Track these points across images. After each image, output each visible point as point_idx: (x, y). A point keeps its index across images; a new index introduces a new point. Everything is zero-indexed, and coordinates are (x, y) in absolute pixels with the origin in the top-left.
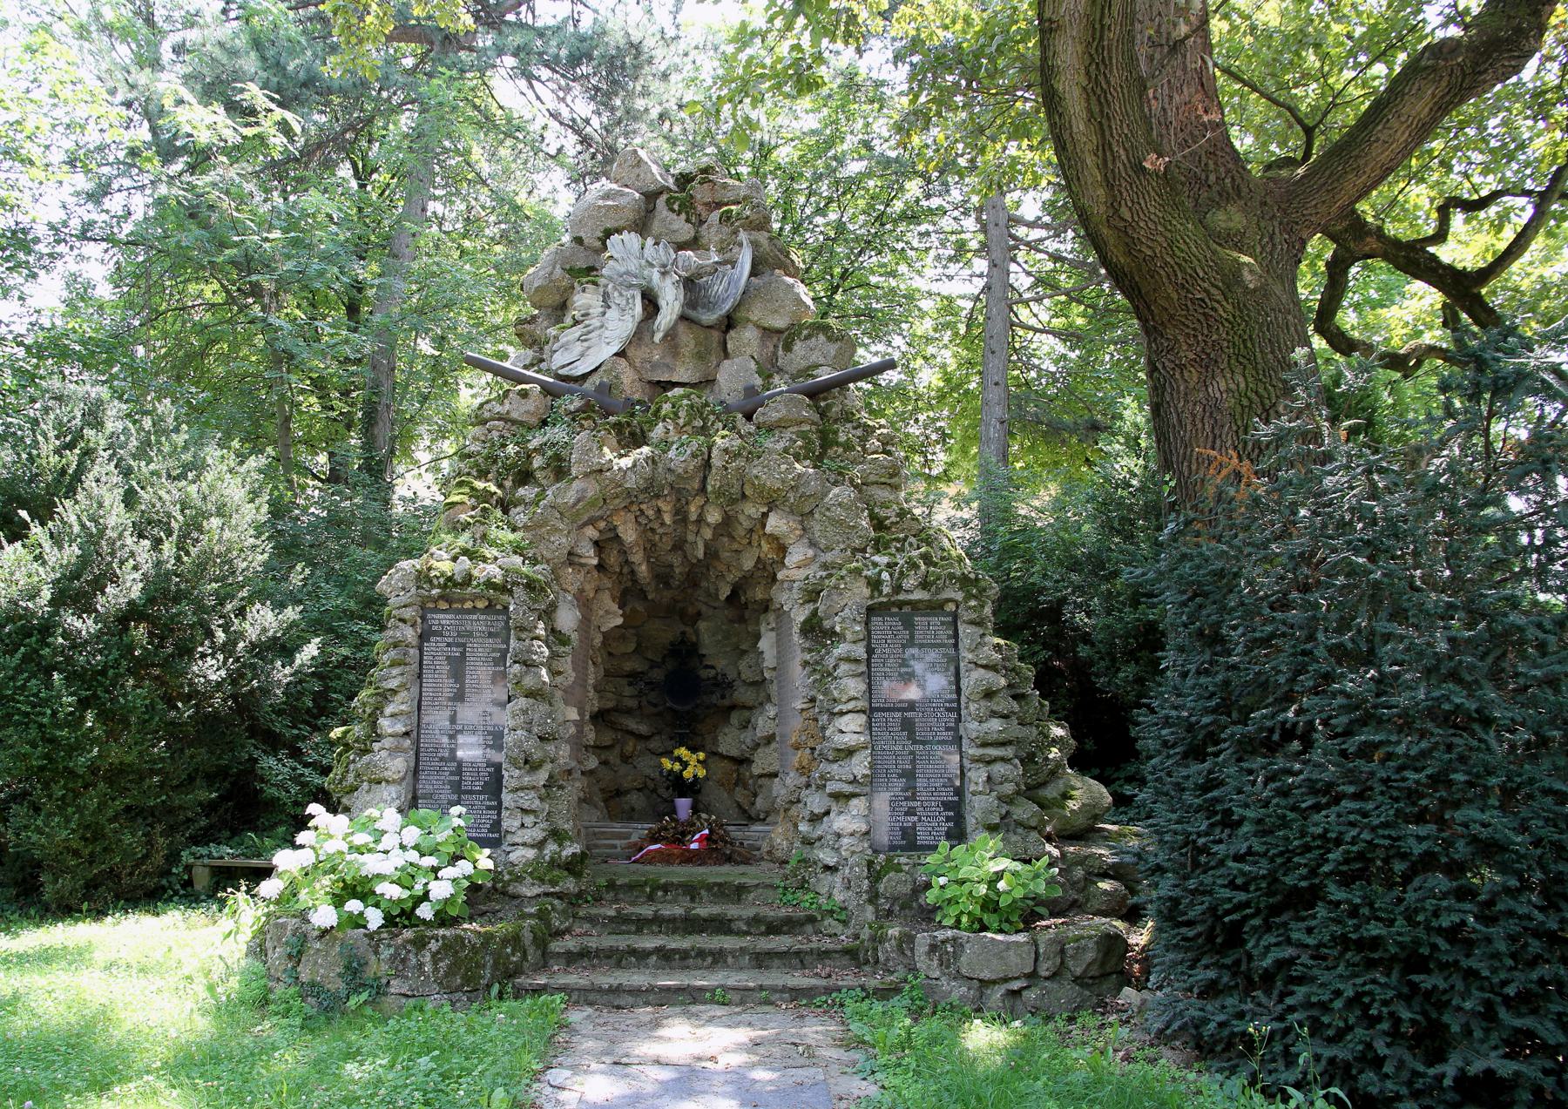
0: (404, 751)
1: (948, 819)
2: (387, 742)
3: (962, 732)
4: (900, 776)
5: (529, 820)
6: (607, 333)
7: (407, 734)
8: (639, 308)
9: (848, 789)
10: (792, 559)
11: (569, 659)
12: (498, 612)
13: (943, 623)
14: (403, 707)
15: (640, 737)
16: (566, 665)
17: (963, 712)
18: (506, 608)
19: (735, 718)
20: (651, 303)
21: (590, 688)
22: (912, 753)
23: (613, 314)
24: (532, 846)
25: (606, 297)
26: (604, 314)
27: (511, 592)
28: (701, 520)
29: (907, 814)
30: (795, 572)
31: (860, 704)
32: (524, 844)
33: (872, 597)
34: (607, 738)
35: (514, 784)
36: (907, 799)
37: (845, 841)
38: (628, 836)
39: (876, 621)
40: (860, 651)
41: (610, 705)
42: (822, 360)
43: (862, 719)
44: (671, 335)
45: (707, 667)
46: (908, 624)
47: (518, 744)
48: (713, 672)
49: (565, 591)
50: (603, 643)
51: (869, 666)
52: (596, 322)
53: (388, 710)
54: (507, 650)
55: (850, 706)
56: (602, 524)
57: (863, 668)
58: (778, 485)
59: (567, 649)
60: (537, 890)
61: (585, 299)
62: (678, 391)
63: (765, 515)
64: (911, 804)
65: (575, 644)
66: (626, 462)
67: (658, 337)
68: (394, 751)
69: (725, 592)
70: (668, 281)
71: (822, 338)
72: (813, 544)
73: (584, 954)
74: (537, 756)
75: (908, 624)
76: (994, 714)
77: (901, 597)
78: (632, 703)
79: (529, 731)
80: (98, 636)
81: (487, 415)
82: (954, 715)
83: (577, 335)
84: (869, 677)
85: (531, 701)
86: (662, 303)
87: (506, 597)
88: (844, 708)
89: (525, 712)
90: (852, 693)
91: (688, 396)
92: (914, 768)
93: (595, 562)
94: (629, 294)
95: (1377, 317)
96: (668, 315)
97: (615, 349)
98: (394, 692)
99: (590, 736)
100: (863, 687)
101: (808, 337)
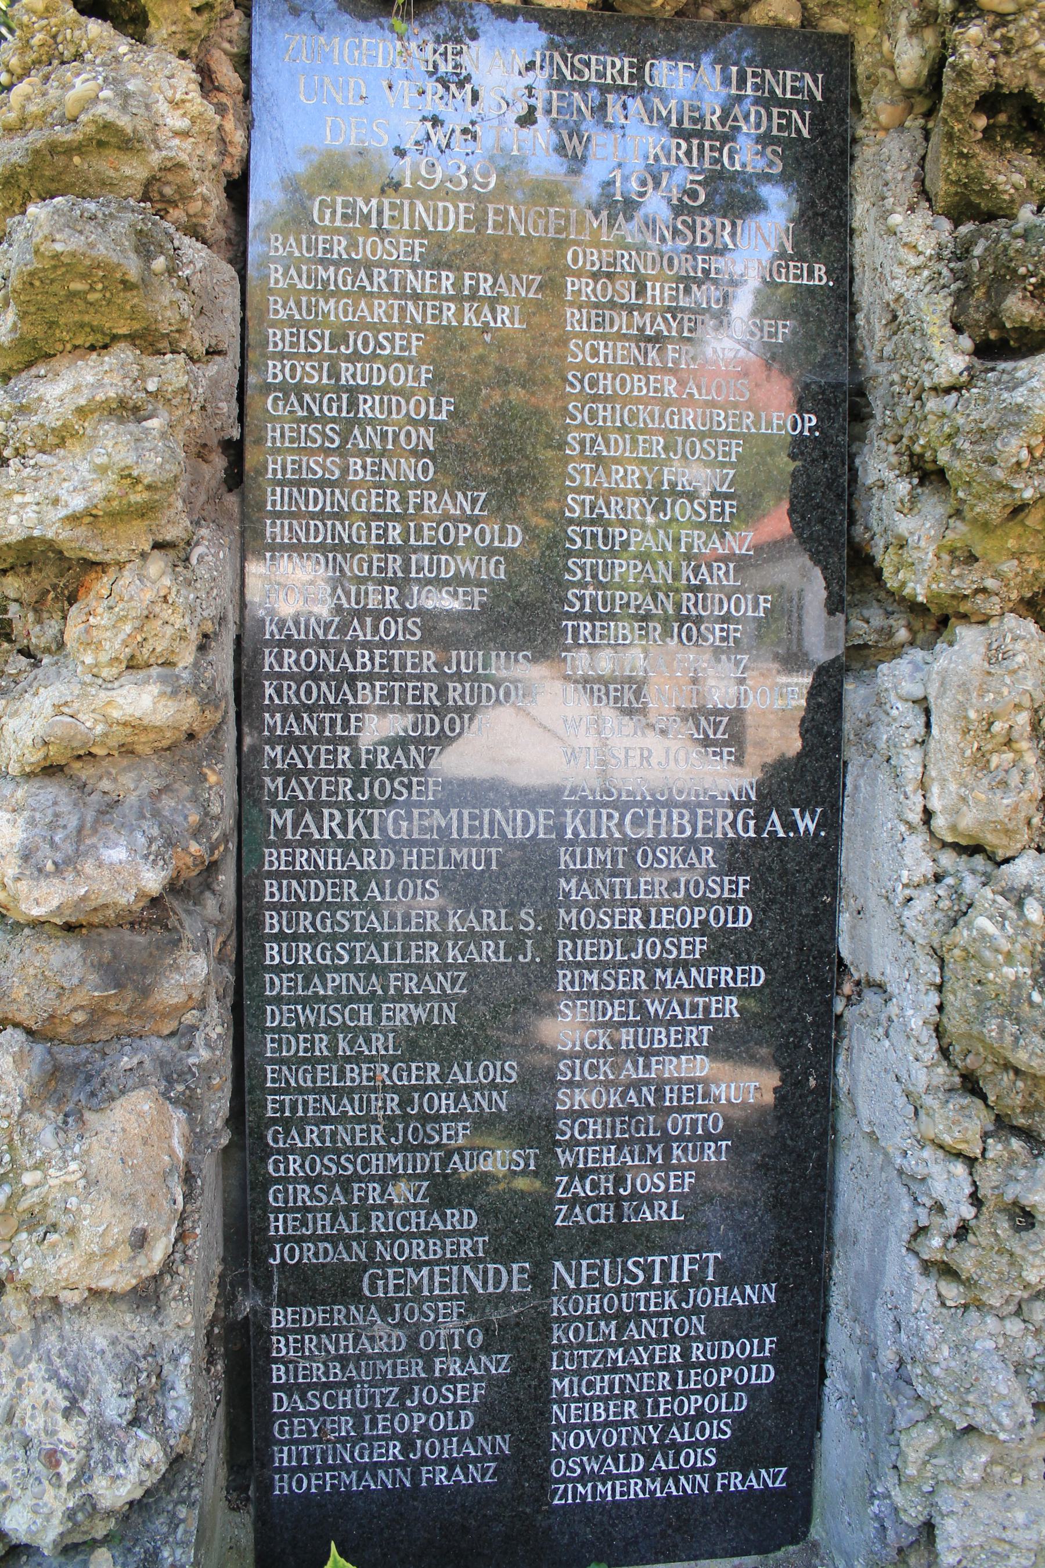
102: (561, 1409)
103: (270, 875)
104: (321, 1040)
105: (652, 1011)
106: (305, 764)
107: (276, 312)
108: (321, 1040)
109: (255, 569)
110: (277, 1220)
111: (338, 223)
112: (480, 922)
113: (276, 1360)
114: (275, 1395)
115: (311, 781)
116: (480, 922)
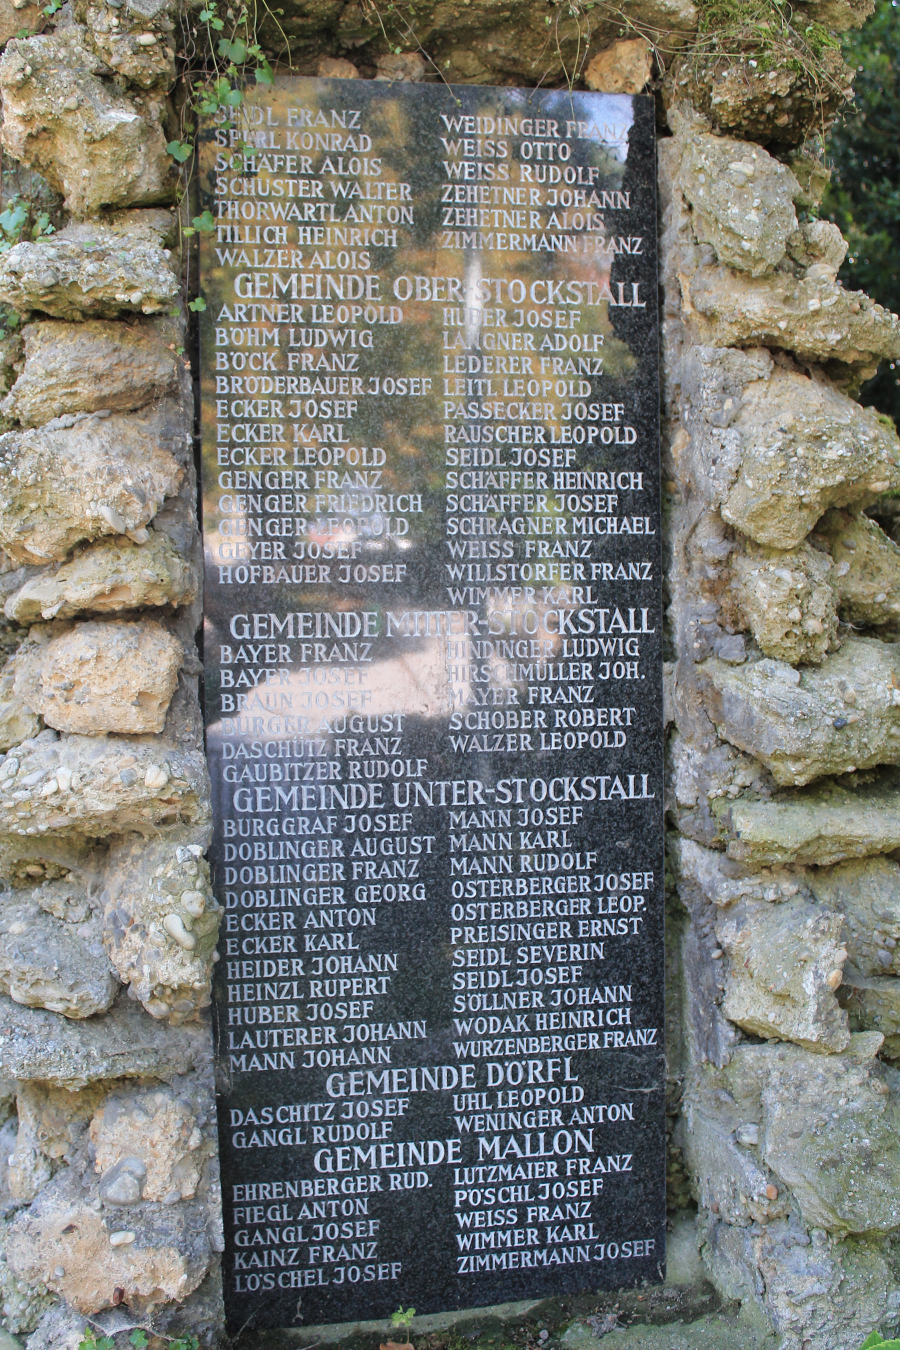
1: (607, 1138)
3: (676, 701)
4: (370, 941)
17: (688, 614)
22: (432, 821)
29: (404, 1130)
31: (138, 575)
43: (156, 657)
51: (196, 342)
55: (81, 584)
57: (157, 360)
66: (726, 98)
82: (635, 624)
88: (47, 594)
90: (95, 510)
92: (441, 899)
95: (169, 567)
100: (161, 476)
102: (491, 860)
103: (225, 691)
104: (297, 310)
105: (453, 552)
106: (251, 659)
107: (227, 682)
108: (297, 310)
109: (215, 728)
110: (233, 966)
111: (258, 295)
112: (331, 944)
113: (225, 691)
114: (227, 869)
115: (256, 672)
116: (331, 944)
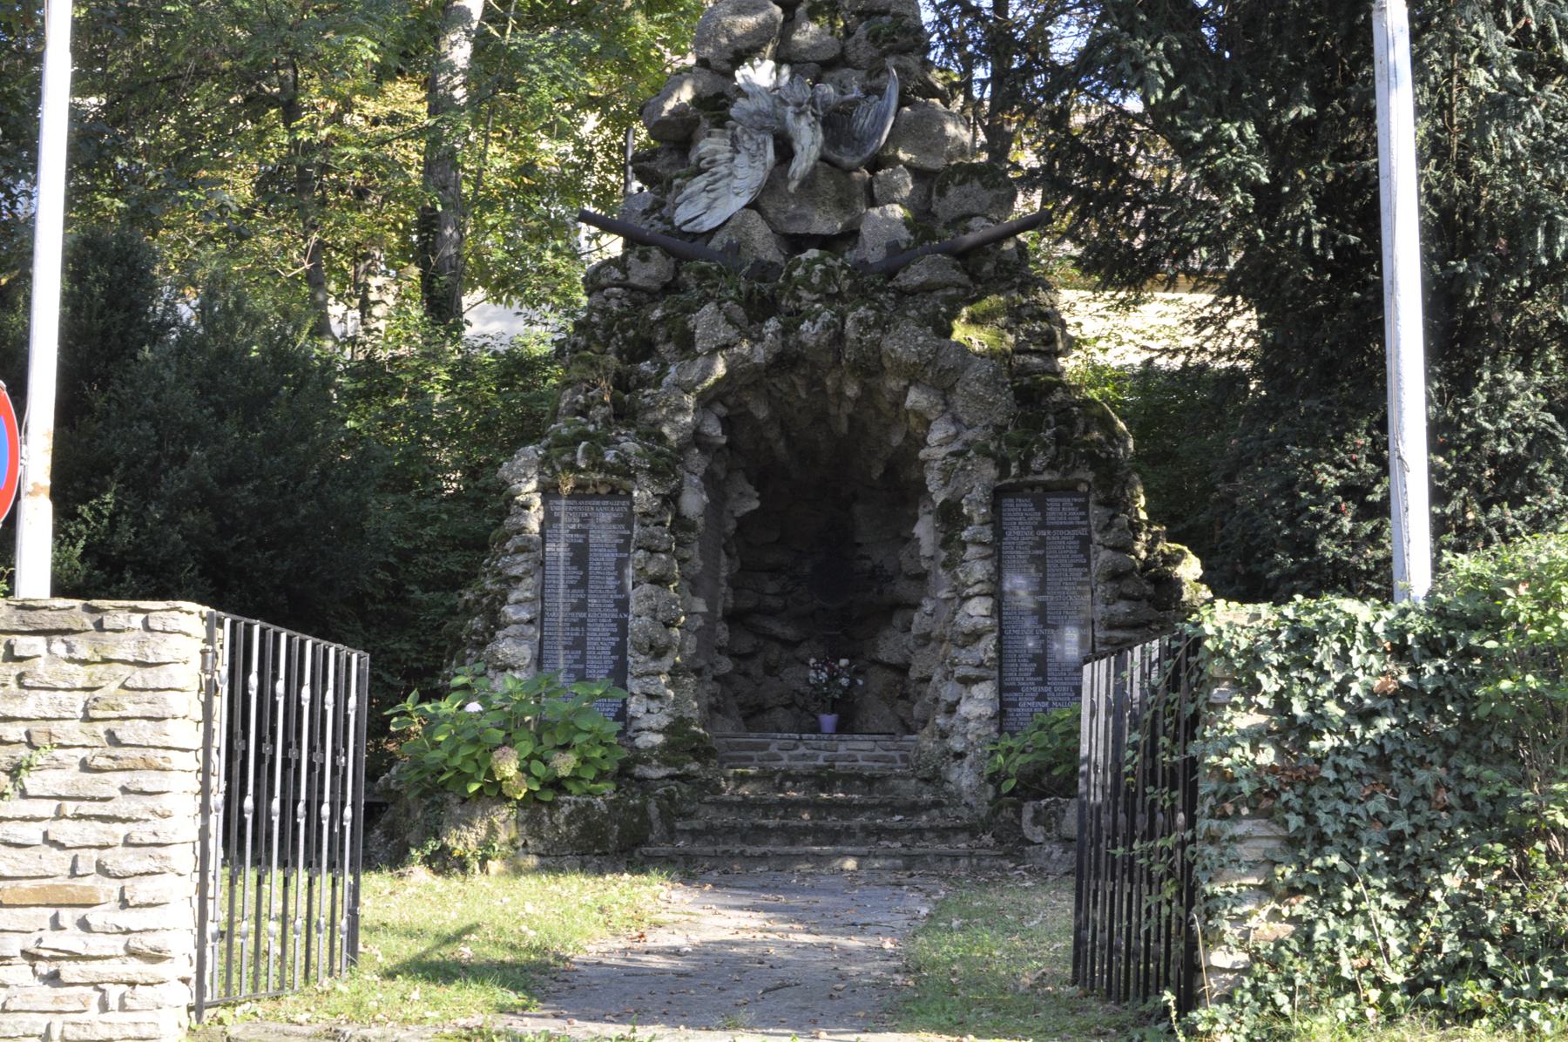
0: (530, 638)
2: (512, 630)
5: (654, 705)
6: (736, 183)
7: (531, 622)
8: (770, 155)
9: (973, 672)
10: (935, 436)
11: (696, 546)
12: (622, 498)
13: (1076, 504)
14: (528, 594)
15: (787, 644)
16: (693, 552)
18: (630, 494)
19: (897, 621)
20: (785, 151)
21: (722, 582)
23: (742, 159)
24: (658, 732)
25: (734, 140)
26: (732, 159)
27: (633, 477)
28: (840, 394)
30: (937, 450)
32: (650, 729)
33: (1000, 479)
34: (746, 644)
35: (640, 669)
36: (1037, 684)
37: (972, 725)
38: (765, 747)
39: (1008, 502)
40: (987, 535)
41: (750, 604)
42: (977, 210)
44: (808, 182)
45: (862, 557)
46: (1041, 507)
47: (643, 629)
48: (869, 564)
49: (692, 473)
50: (738, 529)
52: (723, 170)
53: (513, 597)
54: (630, 536)
55: (976, 589)
56: (731, 400)
58: (915, 359)
59: (692, 535)
60: (662, 772)
61: (711, 145)
62: (813, 253)
63: (906, 388)
64: (1042, 689)
65: (701, 529)
67: (793, 186)
68: (519, 638)
69: (877, 472)
70: (803, 122)
71: (977, 184)
72: (956, 420)
73: (710, 830)
74: (662, 641)
75: (1041, 507)
76: (1123, 596)
77: (1030, 478)
78: (776, 603)
79: (654, 618)
80: (1253, 368)
81: (604, 281)
83: (703, 184)
84: (1000, 561)
85: (656, 587)
86: (798, 148)
87: (628, 483)
88: (971, 591)
89: (649, 597)
91: (821, 260)
93: (723, 441)
94: (760, 138)
96: (802, 163)
97: (744, 200)
98: (518, 579)
99: (723, 633)
101: (961, 183)
